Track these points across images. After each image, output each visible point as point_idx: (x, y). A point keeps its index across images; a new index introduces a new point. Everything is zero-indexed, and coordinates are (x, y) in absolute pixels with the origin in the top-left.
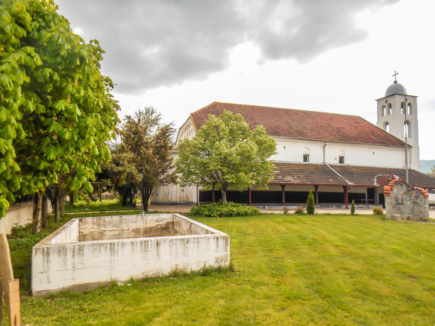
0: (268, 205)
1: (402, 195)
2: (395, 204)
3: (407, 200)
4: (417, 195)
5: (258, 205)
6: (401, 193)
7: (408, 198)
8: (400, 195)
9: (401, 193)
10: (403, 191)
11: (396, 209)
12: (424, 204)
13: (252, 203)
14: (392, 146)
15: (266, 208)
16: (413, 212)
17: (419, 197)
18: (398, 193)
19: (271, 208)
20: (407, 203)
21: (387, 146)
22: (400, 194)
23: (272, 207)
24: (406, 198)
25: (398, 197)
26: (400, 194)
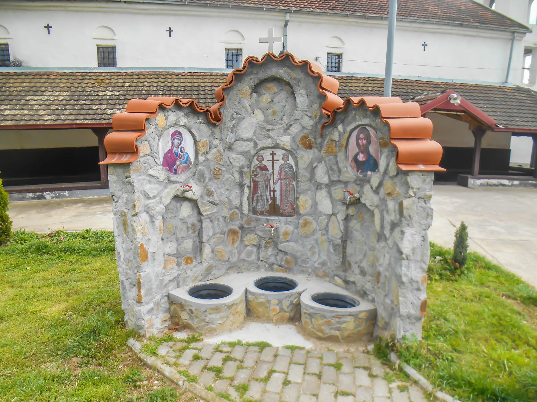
0: (52, 190)
1: (290, 152)
2: (245, 209)
3: (318, 186)
4: (364, 150)
5: (20, 192)
6: (286, 140)
7: (322, 176)
8: (279, 153)
9: (286, 140)
10: (295, 129)
11: (251, 238)
12: (394, 226)
13: (480, 173)
14: (477, 28)
15: (48, 197)
16: (345, 265)
17: (375, 166)
18: (268, 142)
19: (64, 196)
20: (315, 204)
21: (461, 25)
22: (276, 146)
23: (67, 193)
24: (312, 170)
25: (264, 169)
26: (276, 146)
